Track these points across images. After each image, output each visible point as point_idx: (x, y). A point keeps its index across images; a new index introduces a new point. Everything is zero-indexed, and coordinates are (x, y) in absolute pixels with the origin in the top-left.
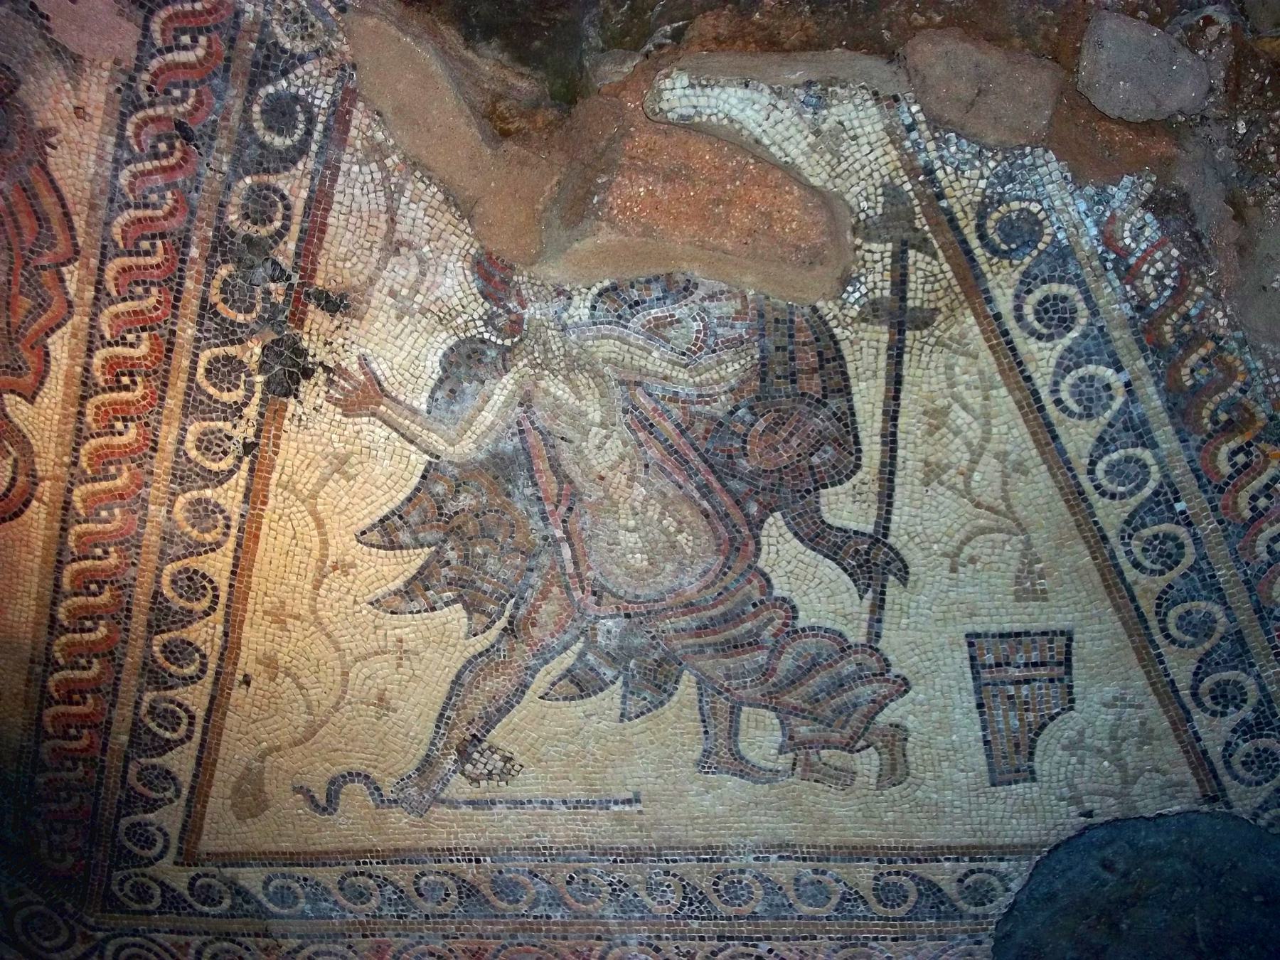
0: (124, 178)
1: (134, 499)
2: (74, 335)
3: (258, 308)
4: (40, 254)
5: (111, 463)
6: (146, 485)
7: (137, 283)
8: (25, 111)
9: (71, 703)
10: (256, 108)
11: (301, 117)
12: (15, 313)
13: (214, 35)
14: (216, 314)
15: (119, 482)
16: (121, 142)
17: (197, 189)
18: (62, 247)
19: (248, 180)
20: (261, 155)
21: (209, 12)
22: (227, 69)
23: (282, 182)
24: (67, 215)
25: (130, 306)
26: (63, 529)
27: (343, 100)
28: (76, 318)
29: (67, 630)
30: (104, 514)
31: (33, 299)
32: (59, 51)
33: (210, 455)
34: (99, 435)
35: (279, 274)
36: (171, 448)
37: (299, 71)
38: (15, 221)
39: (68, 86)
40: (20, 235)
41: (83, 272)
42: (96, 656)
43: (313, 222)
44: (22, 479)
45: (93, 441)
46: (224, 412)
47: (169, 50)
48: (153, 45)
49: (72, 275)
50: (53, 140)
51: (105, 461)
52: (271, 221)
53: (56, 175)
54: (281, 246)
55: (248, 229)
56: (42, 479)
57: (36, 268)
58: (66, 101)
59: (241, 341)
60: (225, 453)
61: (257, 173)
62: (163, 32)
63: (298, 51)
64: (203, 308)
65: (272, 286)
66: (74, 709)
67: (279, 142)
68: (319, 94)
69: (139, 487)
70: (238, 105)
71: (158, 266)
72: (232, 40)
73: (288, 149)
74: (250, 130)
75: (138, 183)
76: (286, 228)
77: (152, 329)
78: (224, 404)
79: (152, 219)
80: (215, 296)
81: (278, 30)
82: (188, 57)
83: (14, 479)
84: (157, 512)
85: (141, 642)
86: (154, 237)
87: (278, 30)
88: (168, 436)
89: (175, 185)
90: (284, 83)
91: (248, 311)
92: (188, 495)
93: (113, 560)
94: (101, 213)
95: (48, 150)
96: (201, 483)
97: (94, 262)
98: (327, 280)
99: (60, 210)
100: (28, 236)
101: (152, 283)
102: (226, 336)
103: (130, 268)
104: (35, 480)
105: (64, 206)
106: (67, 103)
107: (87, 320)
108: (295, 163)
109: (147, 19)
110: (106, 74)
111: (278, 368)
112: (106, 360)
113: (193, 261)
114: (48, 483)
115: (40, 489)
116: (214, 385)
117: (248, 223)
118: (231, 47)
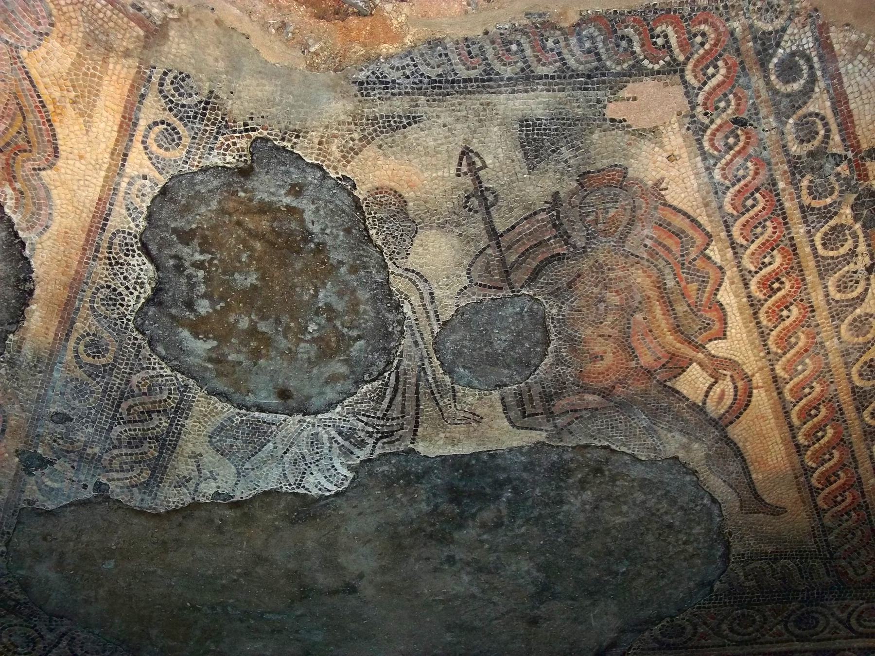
0: (717, 174)
1: (815, 346)
2: (732, 283)
3: (837, 187)
4: (688, 254)
5: (790, 337)
6: (818, 334)
7: (756, 227)
8: (638, 181)
9: (831, 484)
10: (773, 77)
11: (802, 62)
12: (690, 297)
13: (726, 55)
14: (813, 209)
15: (801, 344)
16: (705, 156)
17: (765, 148)
18: (699, 240)
19: (791, 121)
20: (791, 101)
21: (715, 45)
22: (743, 69)
23: (812, 107)
24: (693, 220)
25: (758, 242)
26: (779, 393)
27: (821, 33)
28: (729, 273)
29: (809, 446)
30: (800, 368)
31: (697, 281)
32: (641, 134)
33: (849, 290)
34: (775, 327)
35: (839, 159)
36: (823, 303)
37: (786, 38)
38: (664, 246)
39: (657, 149)
40: (670, 252)
41: (720, 245)
42: (834, 448)
43: (843, 115)
44: (740, 384)
45: (773, 333)
46: (845, 260)
47: (705, 84)
48: (694, 88)
49: (714, 252)
50: (663, 185)
51: (785, 342)
52: (817, 133)
53: (675, 203)
54: (831, 142)
55: (809, 147)
56: (753, 375)
57: (690, 263)
58: (660, 159)
59: (836, 213)
60: (857, 282)
61: (794, 112)
62: (696, 77)
63: (778, 27)
64: (803, 212)
65: (839, 169)
66: (834, 486)
67: (796, 86)
68: (804, 41)
69: (814, 338)
70: (761, 83)
71: (764, 208)
72: (738, 50)
73: (804, 86)
74: (776, 92)
75: (727, 172)
76: (828, 131)
77: (778, 246)
78: (843, 256)
79: (746, 185)
80: (806, 200)
81: (760, 24)
82: (719, 78)
83: (736, 387)
84: (832, 344)
85: (857, 422)
86: (752, 194)
87: (760, 24)
88: (818, 298)
89: (750, 156)
90: (781, 51)
91: (831, 193)
92: (846, 321)
93: (818, 388)
94: (714, 205)
95: (663, 193)
96: (850, 309)
97: (723, 235)
98: (868, 142)
99: (687, 221)
100: (676, 249)
101: (765, 220)
102: (824, 218)
103: (747, 221)
104: (748, 379)
105: (689, 217)
106: (661, 158)
107: (735, 269)
108: (813, 91)
109: (682, 77)
110: (676, 125)
111: (865, 212)
112: (759, 283)
113: (784, 190)
114: (757, 375)
115: (754, 381)
116: (832, 249)
117: (805, 144)
118: (739, 55)
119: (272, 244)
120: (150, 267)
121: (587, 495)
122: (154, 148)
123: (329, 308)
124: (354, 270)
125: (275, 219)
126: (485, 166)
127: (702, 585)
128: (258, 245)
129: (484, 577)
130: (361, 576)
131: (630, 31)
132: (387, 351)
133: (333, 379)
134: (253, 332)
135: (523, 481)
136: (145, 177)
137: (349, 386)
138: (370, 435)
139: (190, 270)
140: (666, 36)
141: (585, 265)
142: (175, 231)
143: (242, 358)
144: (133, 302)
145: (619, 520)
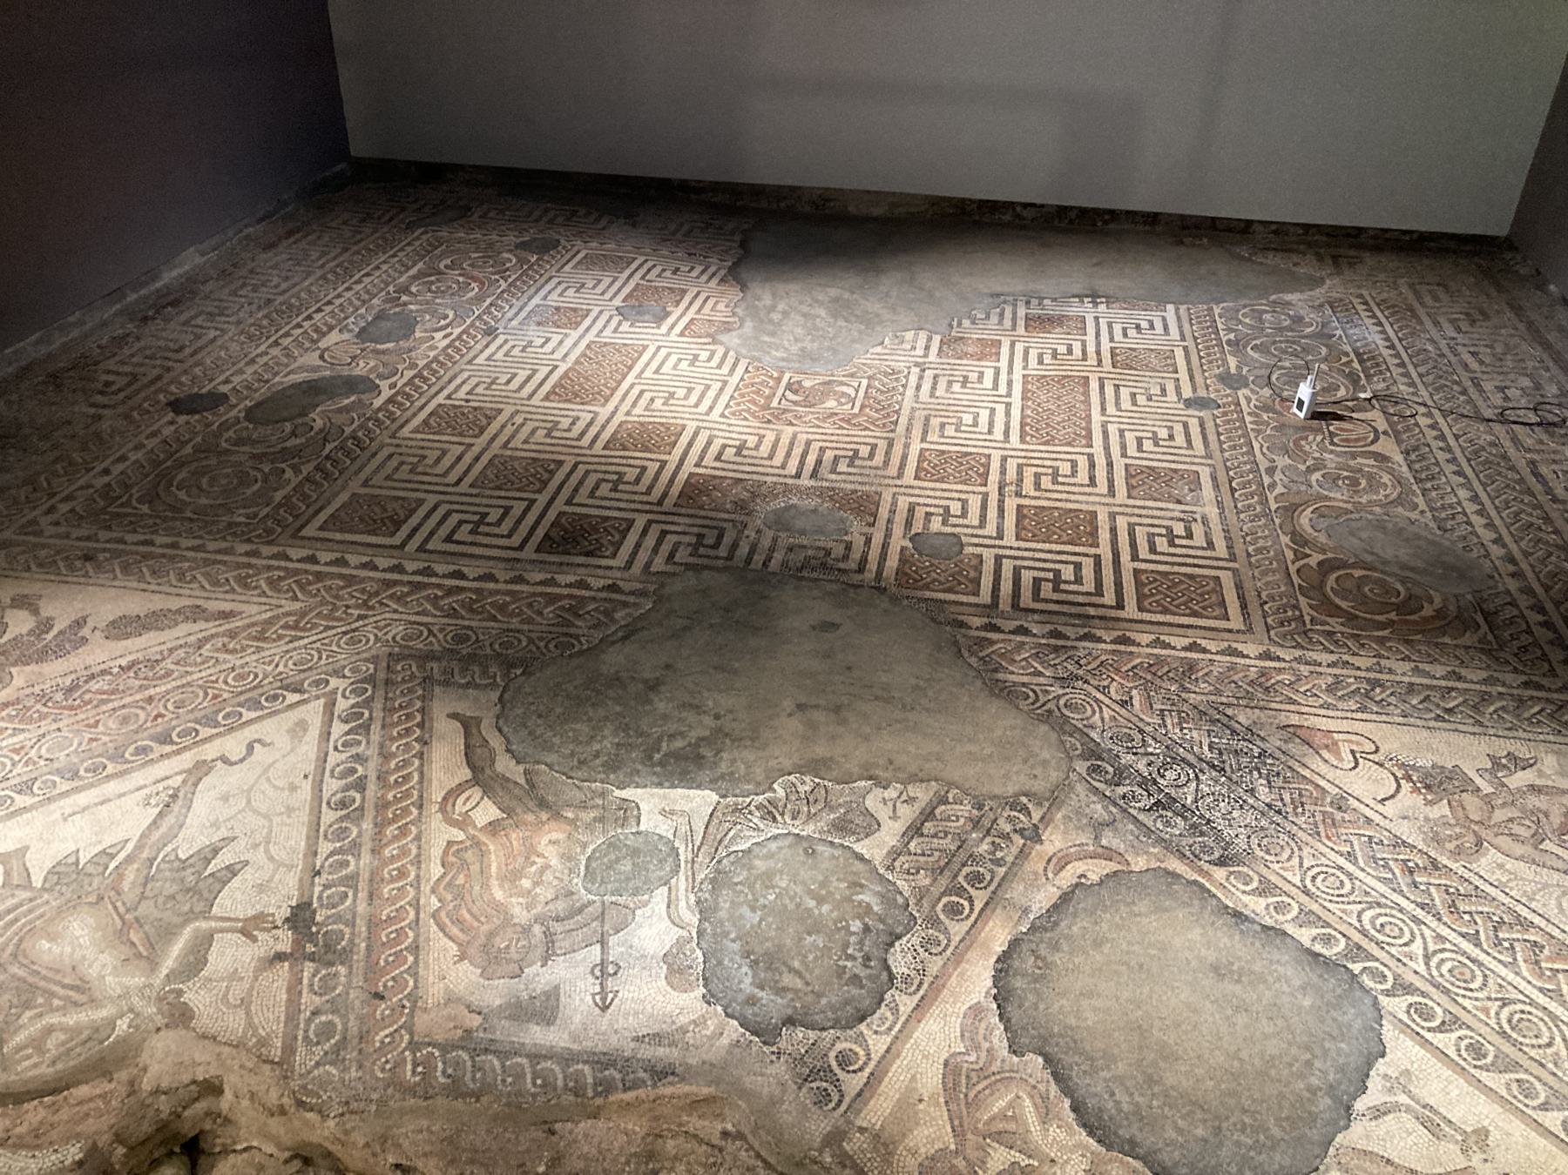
18: (443, 914)
49: (435, 903)
74: (342, 1017)
80: (347, 930)
82: (382, 1034)
97: (422, 915)
119: (784, 963)
120: (890, 962)
121: (596, 747)
122: (862, 1053)
123: (753, 909)
124: (726, 934)
125: (777, 982)
126: (594, 995)
127: (531, 674)
128: (796, 964)
129: (696, 702)
130: (790, 715)
131: (442, 1080)
132: (718, 871)
133: (770, 856)
134: (821, 901)
135: (642, 763)
136: (876, 1032)
137: (756, 850)
138: (750, 813)
139: (858, 955)
140: (414, 1072)
141: (539, 909)
142: (862, 987)
143: (835, 884)
144: (912, 940)
145: (578, 726)
